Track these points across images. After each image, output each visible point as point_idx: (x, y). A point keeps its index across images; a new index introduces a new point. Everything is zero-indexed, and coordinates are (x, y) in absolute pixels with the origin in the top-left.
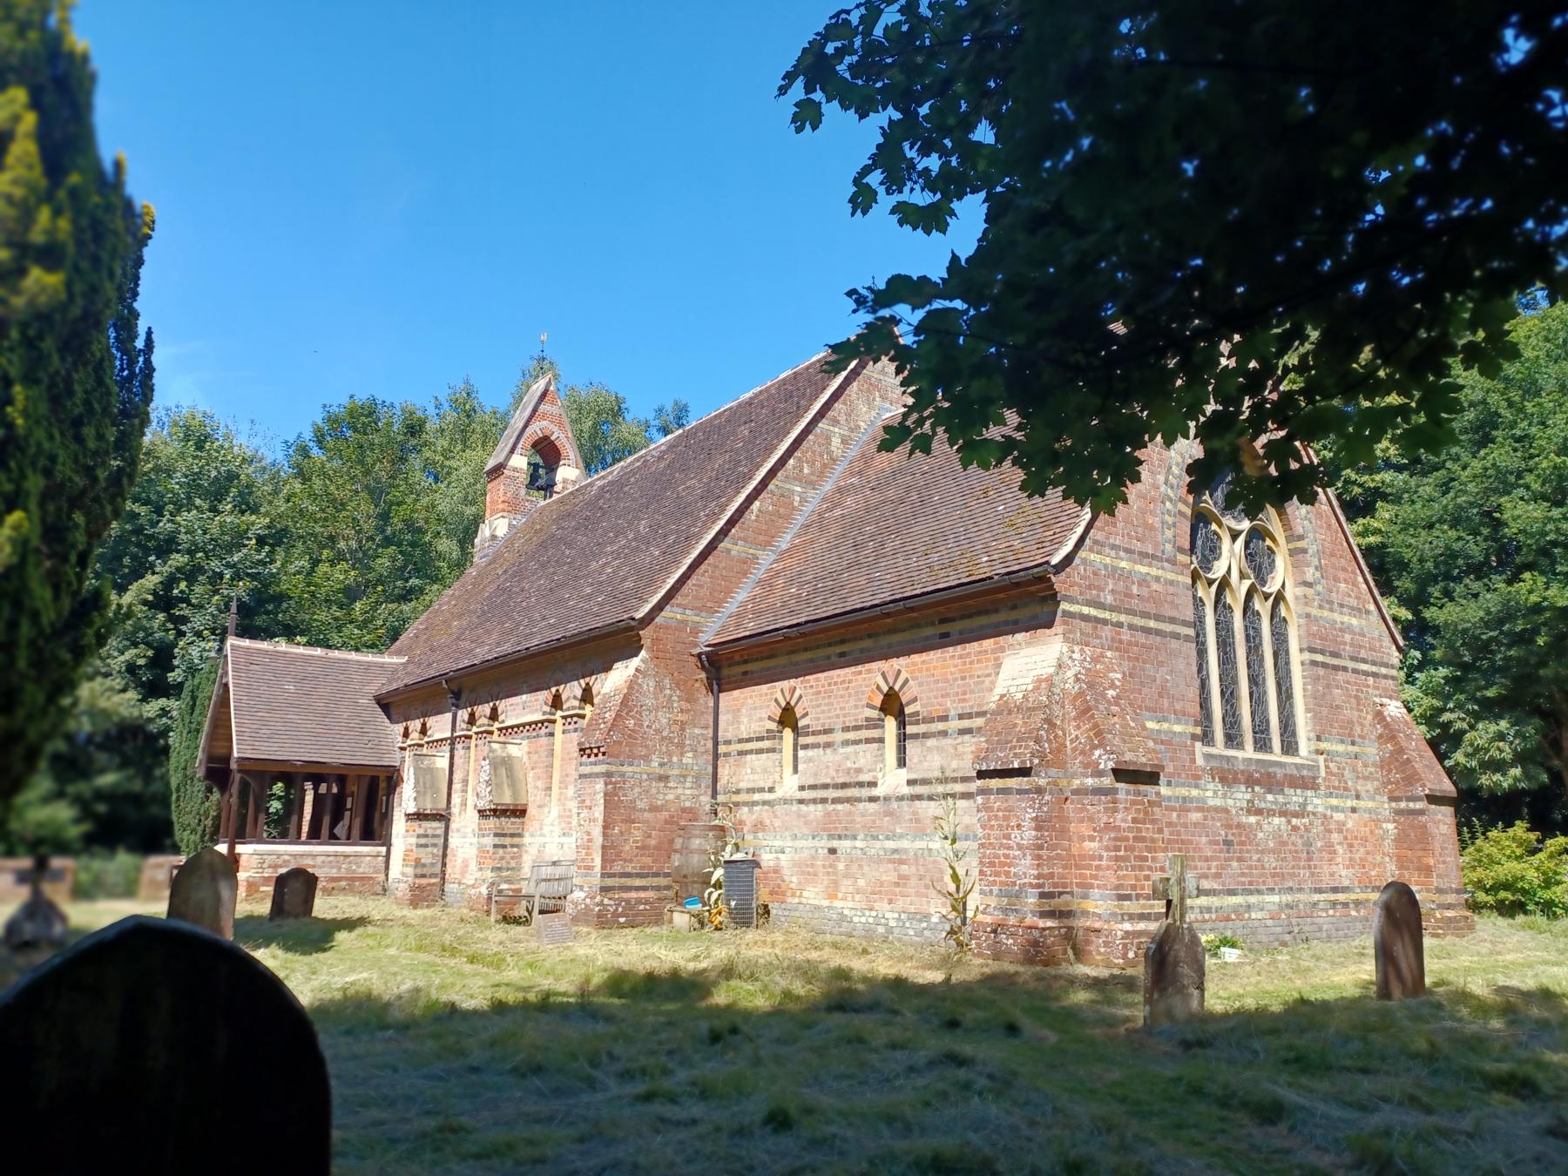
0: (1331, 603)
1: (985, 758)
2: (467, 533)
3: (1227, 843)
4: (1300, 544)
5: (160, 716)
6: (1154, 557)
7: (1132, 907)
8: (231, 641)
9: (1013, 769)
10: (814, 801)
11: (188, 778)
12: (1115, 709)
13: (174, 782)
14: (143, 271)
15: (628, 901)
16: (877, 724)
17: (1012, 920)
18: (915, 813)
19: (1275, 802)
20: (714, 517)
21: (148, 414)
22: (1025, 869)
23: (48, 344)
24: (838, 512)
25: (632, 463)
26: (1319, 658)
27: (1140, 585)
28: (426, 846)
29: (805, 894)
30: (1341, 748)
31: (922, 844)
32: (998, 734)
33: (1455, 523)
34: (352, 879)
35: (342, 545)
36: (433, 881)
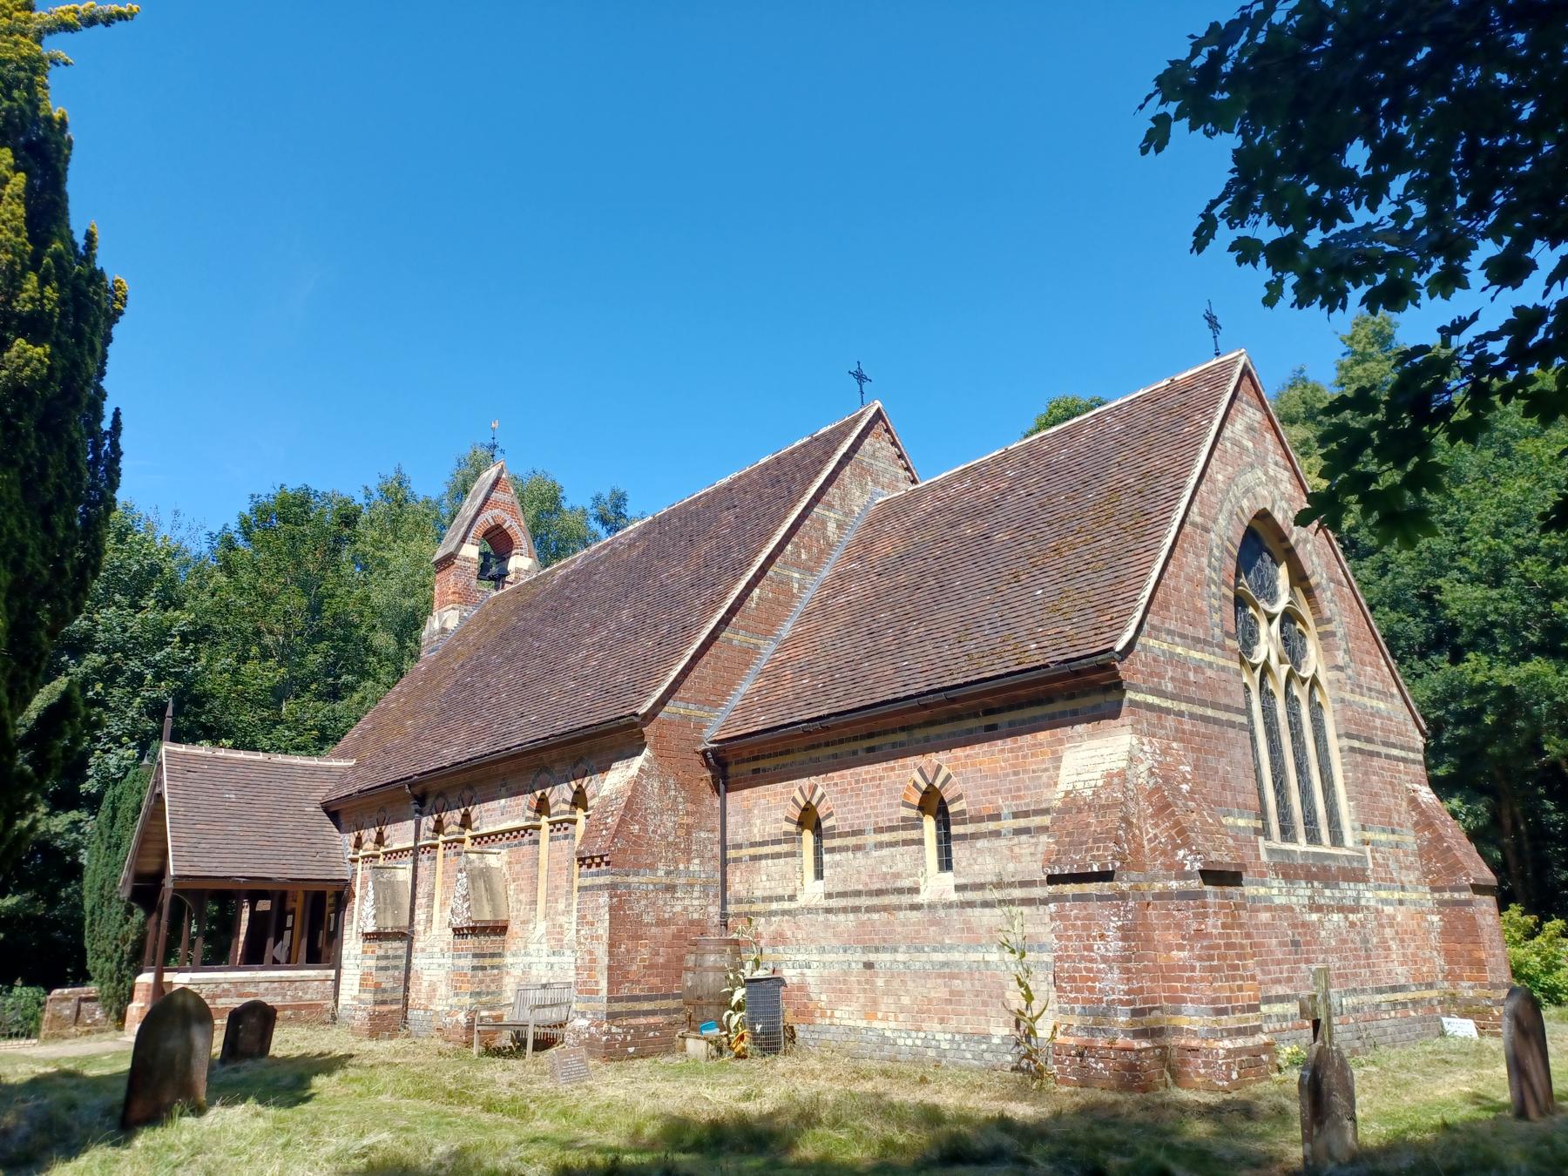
0: (1360, 687)
1: (1057, 862)
2: (409, 625)
3: (1295, 943)
4: (1329, 628)
5: (69, 831)
6: (1205, 642)
7: (1229, 1021)
8: (166, 747)
9: (1093, 873)
10: (845, 910)
11: (105, 899)
12: (1192, 804)
13: (88, 905)
14: (111, 349)
15: (637, 1028)
16: (916, 825)
17: (1100, 1042)
18: (966, 922)
19: (1332, 898)
20: (714, 605)
21: (114, 500)
22: (1112, 984)
23: (26, 424)
24: (842, 599)
25: (595, 552)
26: (1356, 744)
27: (1196, 672)
28: (386, 968)
29: (837, 1014)
30: (1383, 837)
31: (978, 956)
32: (1069, 834)
33: (1394, 606)
34: (299, 1008)
35: (268, 640)
36: (394, 1007)
